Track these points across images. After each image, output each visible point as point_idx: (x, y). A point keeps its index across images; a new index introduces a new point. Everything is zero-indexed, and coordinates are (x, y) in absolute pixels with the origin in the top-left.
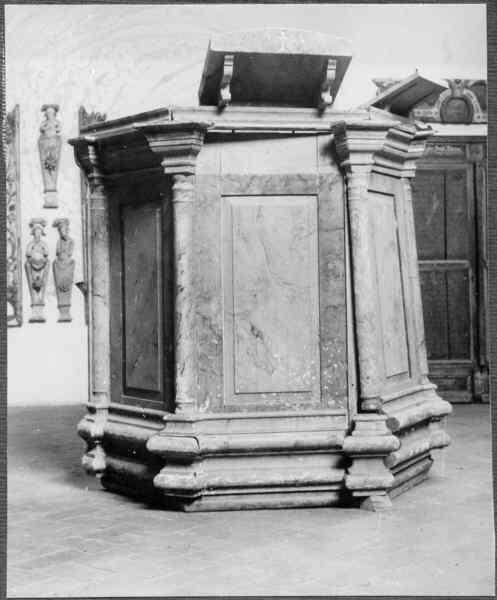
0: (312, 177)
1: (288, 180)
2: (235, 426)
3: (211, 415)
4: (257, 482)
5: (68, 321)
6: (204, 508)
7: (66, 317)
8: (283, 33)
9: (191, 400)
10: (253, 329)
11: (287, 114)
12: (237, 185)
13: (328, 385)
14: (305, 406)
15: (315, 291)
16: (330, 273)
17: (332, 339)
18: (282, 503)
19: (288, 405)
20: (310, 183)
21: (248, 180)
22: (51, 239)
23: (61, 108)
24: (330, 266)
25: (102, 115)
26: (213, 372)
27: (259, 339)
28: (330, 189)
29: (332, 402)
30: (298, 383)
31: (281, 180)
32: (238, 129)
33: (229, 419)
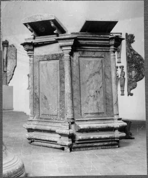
0: (58, 54)
1: (53, 55)
2: (40, 123)
3: (36, 120)
4: (43, 139)
5: (124, 95)
6: (34, 144)
7: (123, 94)
8: (37, 16)
9: (31, 115)
10: (45, 97)
11: (50, 37)
12: (42, 58)
13: (61, 114)
14: (56, 119)
15: (59, 87)
16: (62, 82)
17: (62, 101)
18: (50, 146)
19: (52, 119)
20: (57, 56)
21: (44, 56)
22: (119, 71)
23: (122, 33)
24: (62, 80)
25: (132, 34)
26: (37, 108)
27: (46, 100)
28: (62, 57)
29: (62, 119)
30: (55, 113)
31: (51, 56)
32: (81, 39)
33: (39, 121)
